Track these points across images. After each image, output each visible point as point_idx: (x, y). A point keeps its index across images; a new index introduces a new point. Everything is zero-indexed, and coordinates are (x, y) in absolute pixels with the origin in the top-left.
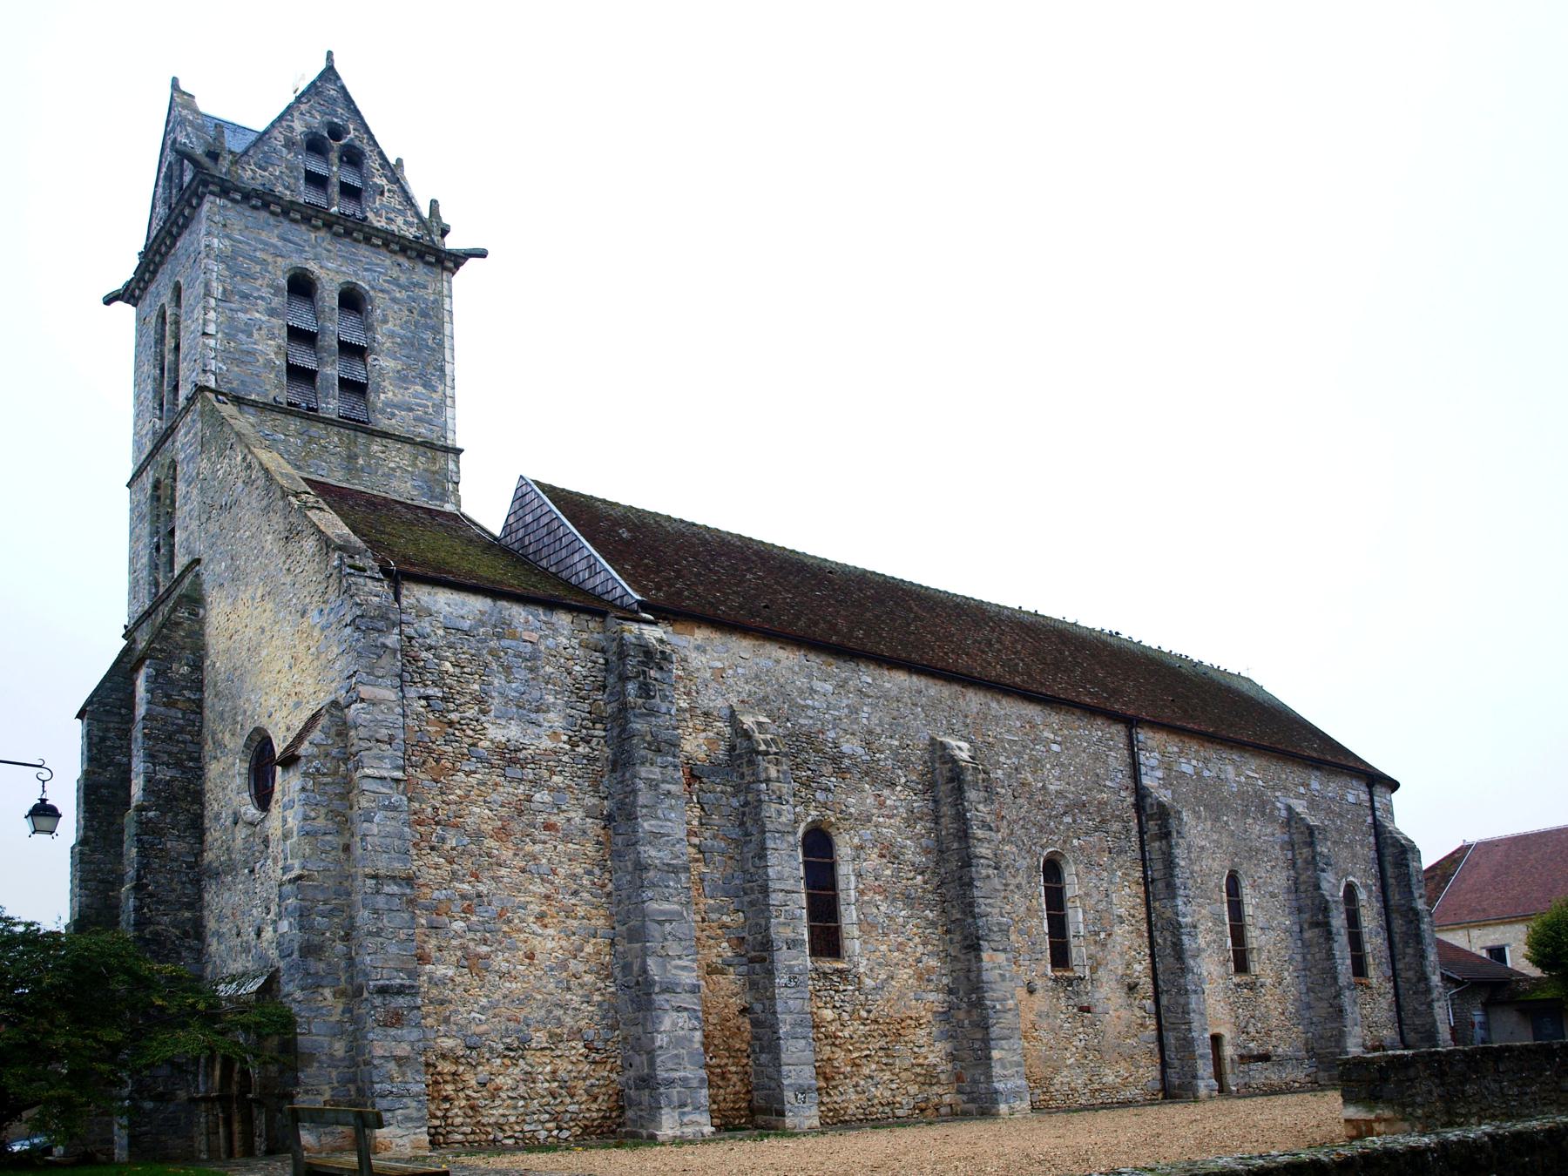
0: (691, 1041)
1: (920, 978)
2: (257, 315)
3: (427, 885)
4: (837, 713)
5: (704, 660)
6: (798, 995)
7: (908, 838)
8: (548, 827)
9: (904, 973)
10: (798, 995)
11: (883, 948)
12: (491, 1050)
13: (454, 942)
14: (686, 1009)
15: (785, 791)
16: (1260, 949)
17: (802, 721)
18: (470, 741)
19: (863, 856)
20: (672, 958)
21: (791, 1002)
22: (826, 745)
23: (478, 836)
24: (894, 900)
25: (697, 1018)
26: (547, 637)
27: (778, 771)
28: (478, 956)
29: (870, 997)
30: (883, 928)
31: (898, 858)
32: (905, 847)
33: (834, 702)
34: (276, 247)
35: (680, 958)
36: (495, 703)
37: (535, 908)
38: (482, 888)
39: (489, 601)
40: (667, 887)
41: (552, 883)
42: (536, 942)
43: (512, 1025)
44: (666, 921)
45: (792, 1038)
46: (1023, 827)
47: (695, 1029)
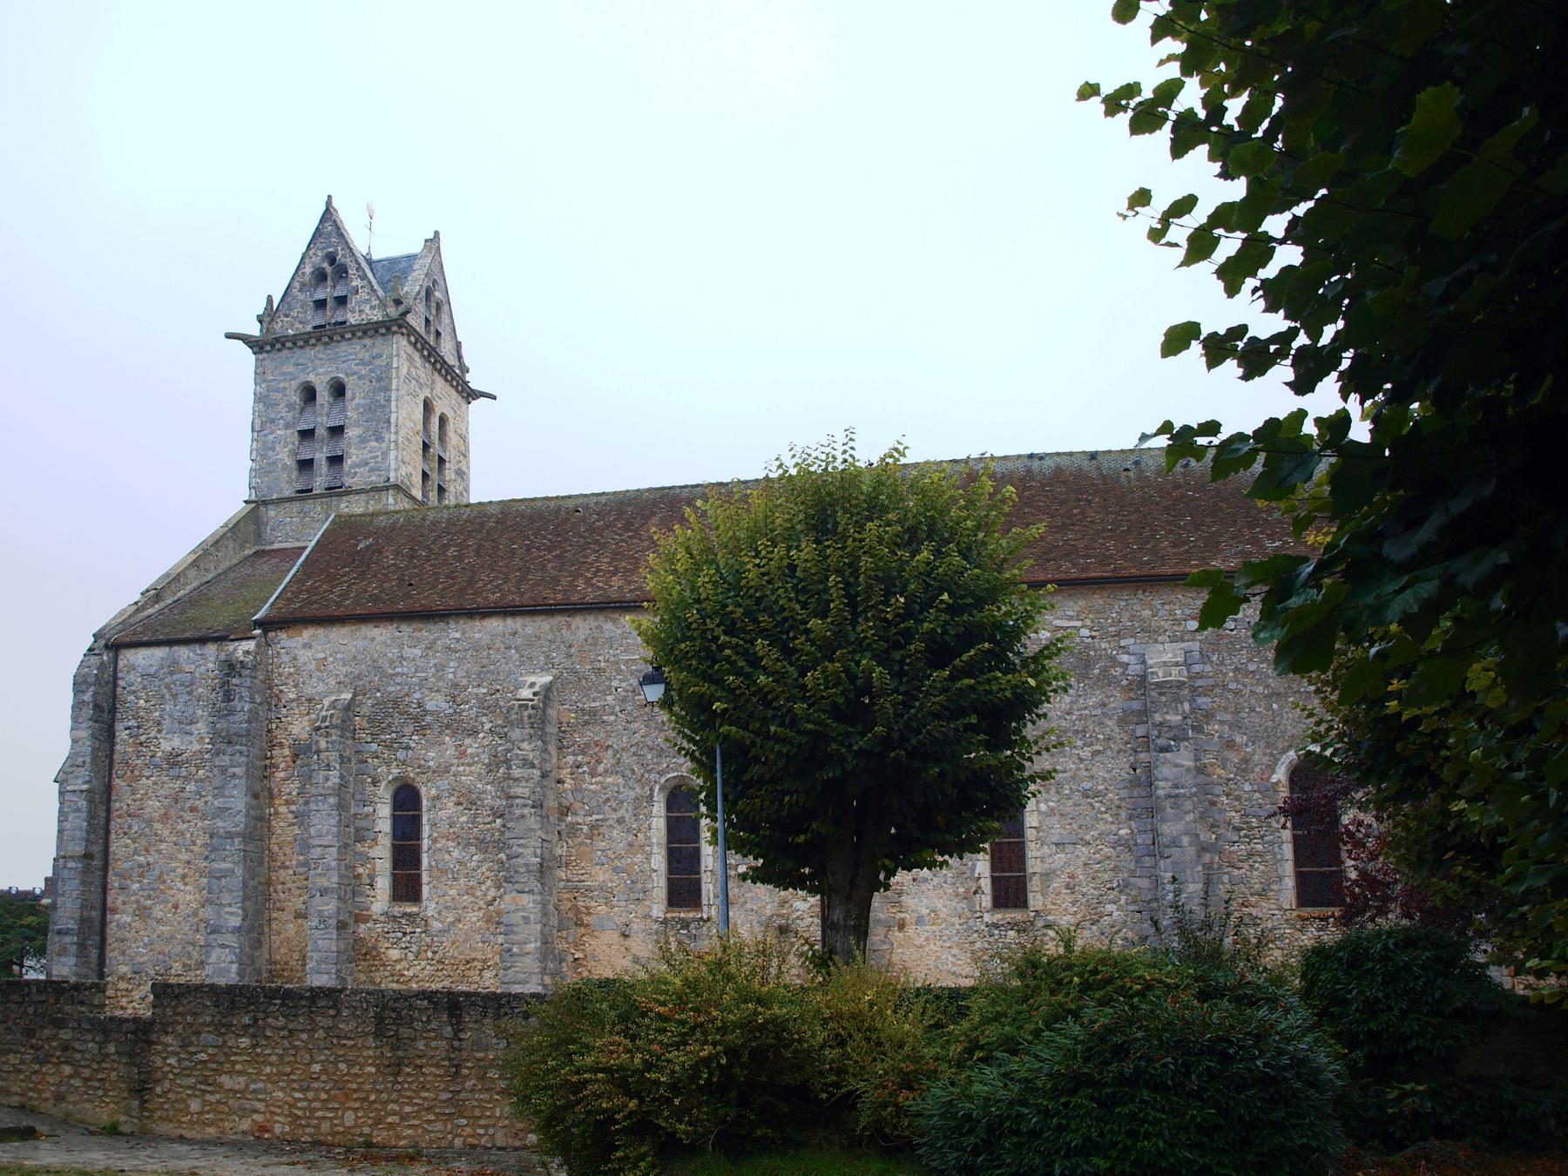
0: (229, 971)
1: (489, 921)
2: (279, 432)
3: (120, 859)
4: (423, 674)
5: (310, 654)
6: (327, 936)
7: (488, 784)
8: (193, 809)
9: (474, 917)
10: (327, 936)
11: (452, 892)
12: (147, 974)
13: (133, 898)
14: (228, 946)
15: (331, 759)
16: (1047, 876)
17: (391, 689)
18: (150, 754)
19: (439, 805)
20: (224, 906)
21: (320, 942)
22: (410, 707)
23: (150, 822)
24: (469, 844)
25: (235, 954)
26: (200, 665)
27: (327, 742)
28: (145, 908)
29: (435, 939)
30: (453, 872)
31: (475, 804)
32: (484, 792)
33: (421, 665)
34: (291, 374)
35: (230, 905)
36: (166, 724)
37: (180, 871)
38: (150, 859)
39: (167, 649)
40: (225, 850)
41: (192, 852)
42: (180, 896)
43: (161, 957)
44: (222, 877)
45: (317, 973)
46: (635, 754)
47: (232, 962)
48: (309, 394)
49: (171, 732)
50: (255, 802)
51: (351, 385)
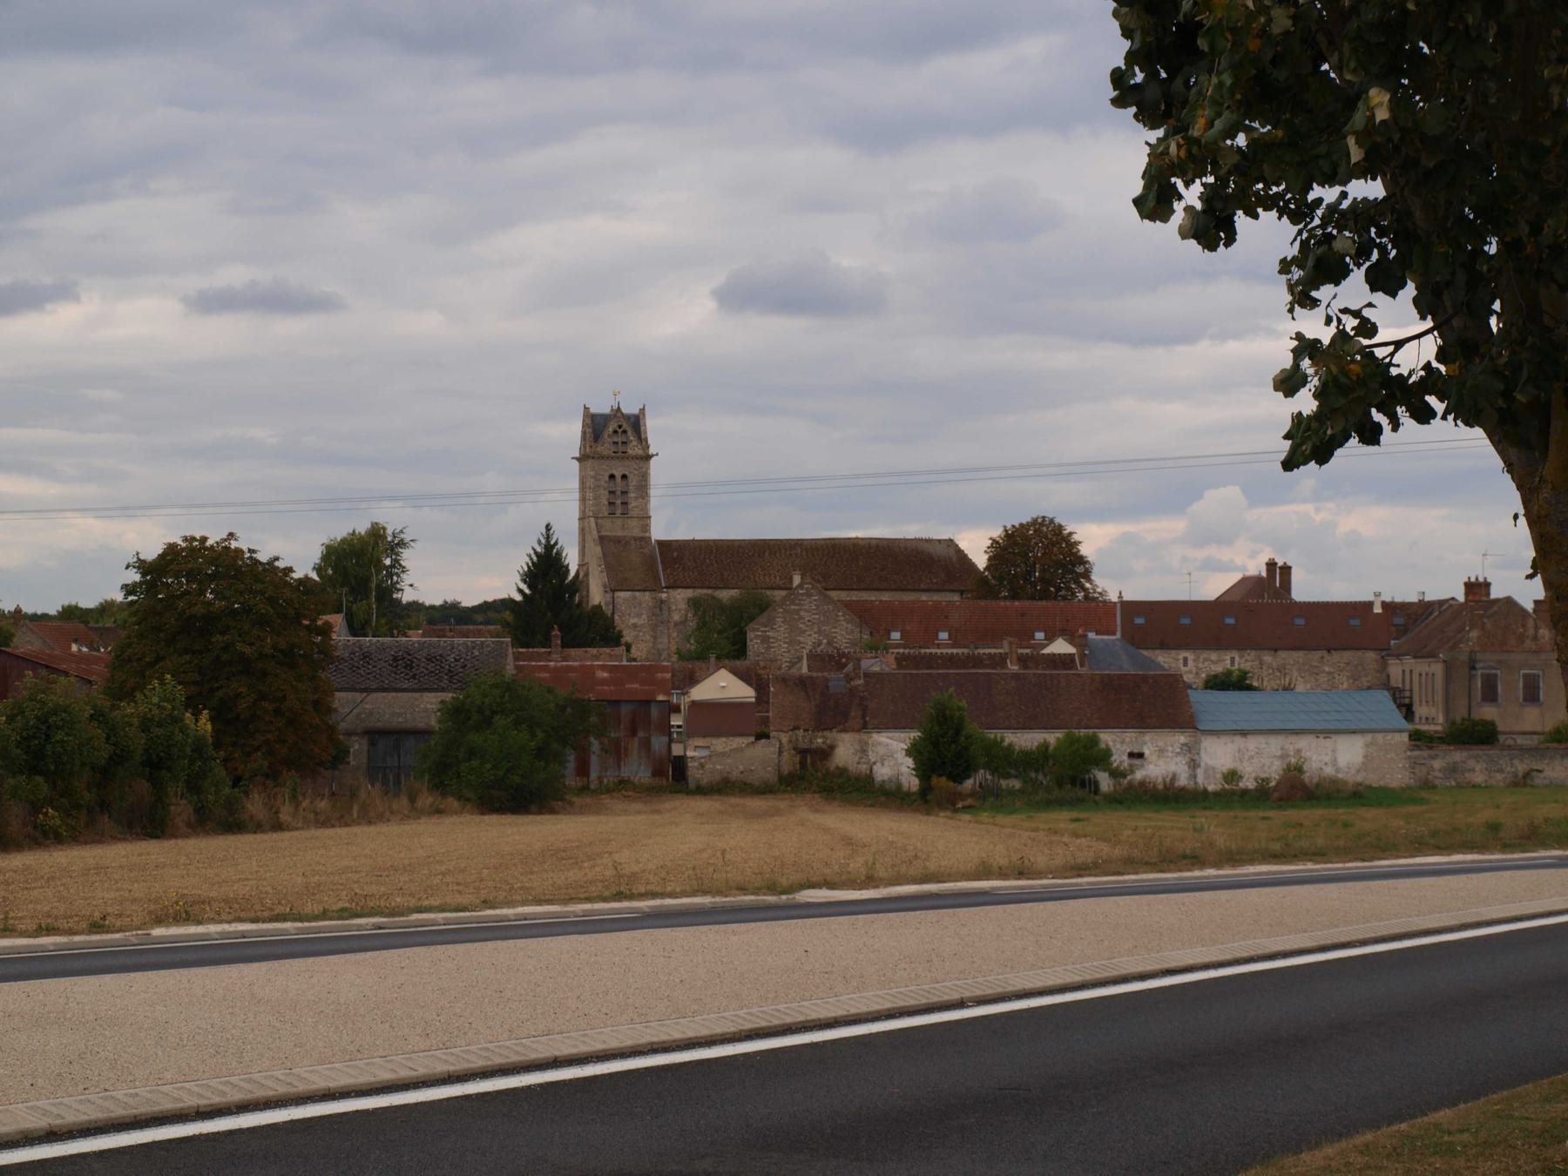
36: (632, 615)
48: (612, 477)
49: (634, 617)
50: (1292, 769)
51: (631, 477)
